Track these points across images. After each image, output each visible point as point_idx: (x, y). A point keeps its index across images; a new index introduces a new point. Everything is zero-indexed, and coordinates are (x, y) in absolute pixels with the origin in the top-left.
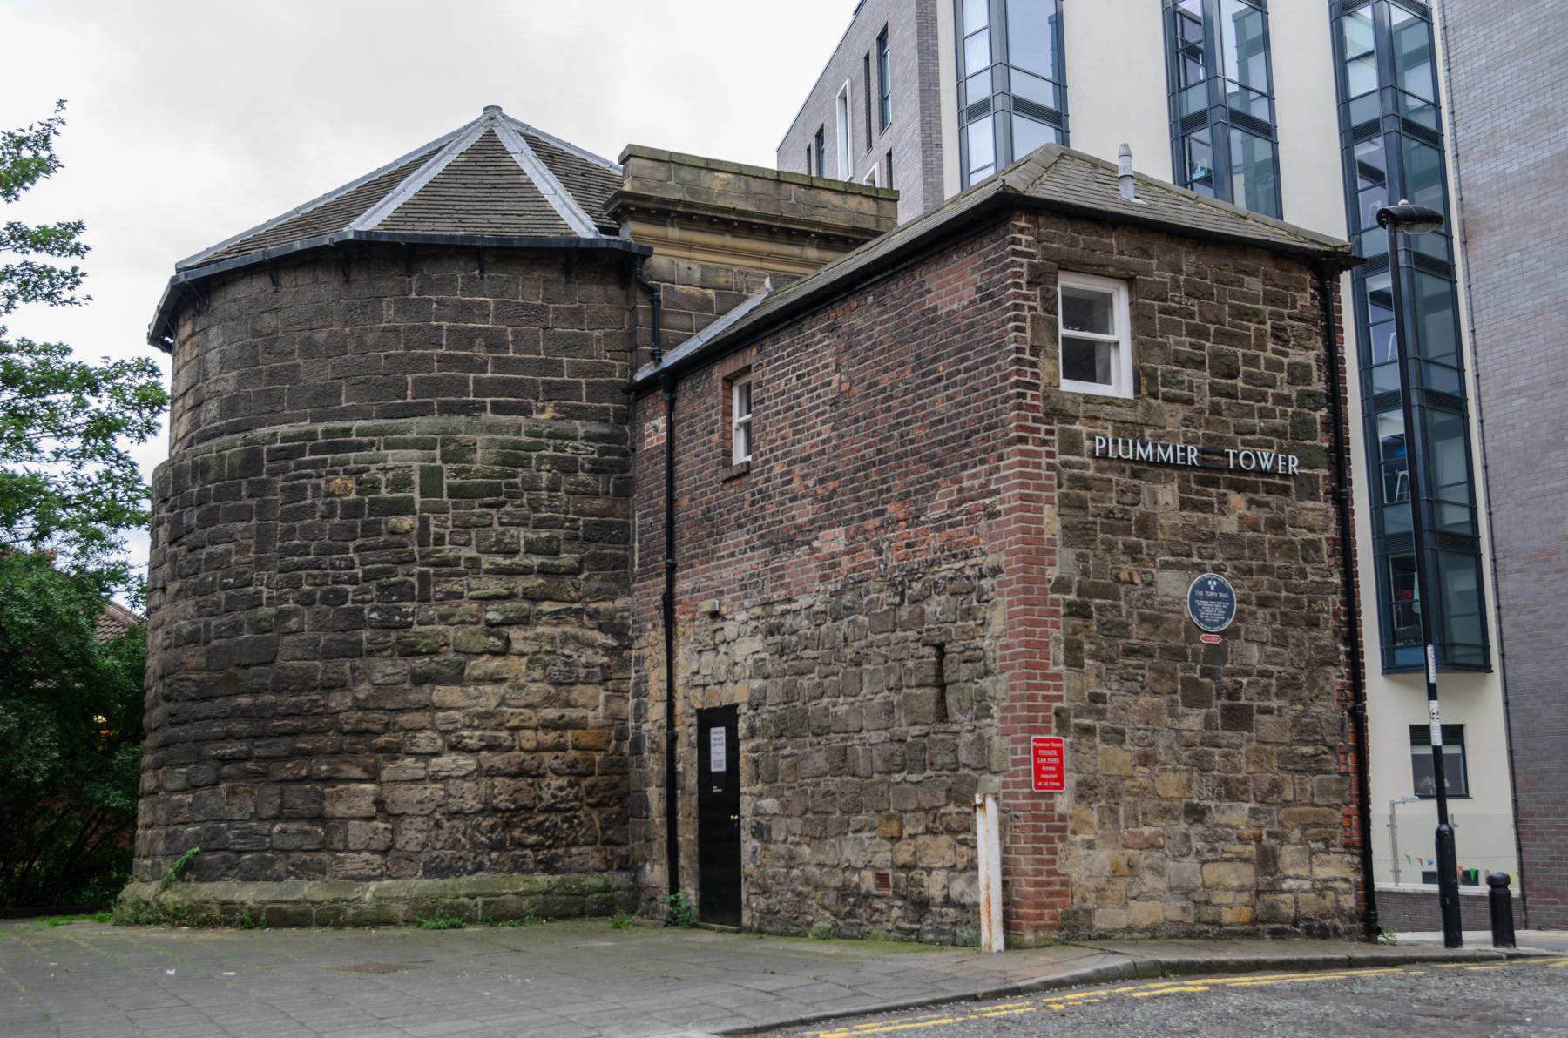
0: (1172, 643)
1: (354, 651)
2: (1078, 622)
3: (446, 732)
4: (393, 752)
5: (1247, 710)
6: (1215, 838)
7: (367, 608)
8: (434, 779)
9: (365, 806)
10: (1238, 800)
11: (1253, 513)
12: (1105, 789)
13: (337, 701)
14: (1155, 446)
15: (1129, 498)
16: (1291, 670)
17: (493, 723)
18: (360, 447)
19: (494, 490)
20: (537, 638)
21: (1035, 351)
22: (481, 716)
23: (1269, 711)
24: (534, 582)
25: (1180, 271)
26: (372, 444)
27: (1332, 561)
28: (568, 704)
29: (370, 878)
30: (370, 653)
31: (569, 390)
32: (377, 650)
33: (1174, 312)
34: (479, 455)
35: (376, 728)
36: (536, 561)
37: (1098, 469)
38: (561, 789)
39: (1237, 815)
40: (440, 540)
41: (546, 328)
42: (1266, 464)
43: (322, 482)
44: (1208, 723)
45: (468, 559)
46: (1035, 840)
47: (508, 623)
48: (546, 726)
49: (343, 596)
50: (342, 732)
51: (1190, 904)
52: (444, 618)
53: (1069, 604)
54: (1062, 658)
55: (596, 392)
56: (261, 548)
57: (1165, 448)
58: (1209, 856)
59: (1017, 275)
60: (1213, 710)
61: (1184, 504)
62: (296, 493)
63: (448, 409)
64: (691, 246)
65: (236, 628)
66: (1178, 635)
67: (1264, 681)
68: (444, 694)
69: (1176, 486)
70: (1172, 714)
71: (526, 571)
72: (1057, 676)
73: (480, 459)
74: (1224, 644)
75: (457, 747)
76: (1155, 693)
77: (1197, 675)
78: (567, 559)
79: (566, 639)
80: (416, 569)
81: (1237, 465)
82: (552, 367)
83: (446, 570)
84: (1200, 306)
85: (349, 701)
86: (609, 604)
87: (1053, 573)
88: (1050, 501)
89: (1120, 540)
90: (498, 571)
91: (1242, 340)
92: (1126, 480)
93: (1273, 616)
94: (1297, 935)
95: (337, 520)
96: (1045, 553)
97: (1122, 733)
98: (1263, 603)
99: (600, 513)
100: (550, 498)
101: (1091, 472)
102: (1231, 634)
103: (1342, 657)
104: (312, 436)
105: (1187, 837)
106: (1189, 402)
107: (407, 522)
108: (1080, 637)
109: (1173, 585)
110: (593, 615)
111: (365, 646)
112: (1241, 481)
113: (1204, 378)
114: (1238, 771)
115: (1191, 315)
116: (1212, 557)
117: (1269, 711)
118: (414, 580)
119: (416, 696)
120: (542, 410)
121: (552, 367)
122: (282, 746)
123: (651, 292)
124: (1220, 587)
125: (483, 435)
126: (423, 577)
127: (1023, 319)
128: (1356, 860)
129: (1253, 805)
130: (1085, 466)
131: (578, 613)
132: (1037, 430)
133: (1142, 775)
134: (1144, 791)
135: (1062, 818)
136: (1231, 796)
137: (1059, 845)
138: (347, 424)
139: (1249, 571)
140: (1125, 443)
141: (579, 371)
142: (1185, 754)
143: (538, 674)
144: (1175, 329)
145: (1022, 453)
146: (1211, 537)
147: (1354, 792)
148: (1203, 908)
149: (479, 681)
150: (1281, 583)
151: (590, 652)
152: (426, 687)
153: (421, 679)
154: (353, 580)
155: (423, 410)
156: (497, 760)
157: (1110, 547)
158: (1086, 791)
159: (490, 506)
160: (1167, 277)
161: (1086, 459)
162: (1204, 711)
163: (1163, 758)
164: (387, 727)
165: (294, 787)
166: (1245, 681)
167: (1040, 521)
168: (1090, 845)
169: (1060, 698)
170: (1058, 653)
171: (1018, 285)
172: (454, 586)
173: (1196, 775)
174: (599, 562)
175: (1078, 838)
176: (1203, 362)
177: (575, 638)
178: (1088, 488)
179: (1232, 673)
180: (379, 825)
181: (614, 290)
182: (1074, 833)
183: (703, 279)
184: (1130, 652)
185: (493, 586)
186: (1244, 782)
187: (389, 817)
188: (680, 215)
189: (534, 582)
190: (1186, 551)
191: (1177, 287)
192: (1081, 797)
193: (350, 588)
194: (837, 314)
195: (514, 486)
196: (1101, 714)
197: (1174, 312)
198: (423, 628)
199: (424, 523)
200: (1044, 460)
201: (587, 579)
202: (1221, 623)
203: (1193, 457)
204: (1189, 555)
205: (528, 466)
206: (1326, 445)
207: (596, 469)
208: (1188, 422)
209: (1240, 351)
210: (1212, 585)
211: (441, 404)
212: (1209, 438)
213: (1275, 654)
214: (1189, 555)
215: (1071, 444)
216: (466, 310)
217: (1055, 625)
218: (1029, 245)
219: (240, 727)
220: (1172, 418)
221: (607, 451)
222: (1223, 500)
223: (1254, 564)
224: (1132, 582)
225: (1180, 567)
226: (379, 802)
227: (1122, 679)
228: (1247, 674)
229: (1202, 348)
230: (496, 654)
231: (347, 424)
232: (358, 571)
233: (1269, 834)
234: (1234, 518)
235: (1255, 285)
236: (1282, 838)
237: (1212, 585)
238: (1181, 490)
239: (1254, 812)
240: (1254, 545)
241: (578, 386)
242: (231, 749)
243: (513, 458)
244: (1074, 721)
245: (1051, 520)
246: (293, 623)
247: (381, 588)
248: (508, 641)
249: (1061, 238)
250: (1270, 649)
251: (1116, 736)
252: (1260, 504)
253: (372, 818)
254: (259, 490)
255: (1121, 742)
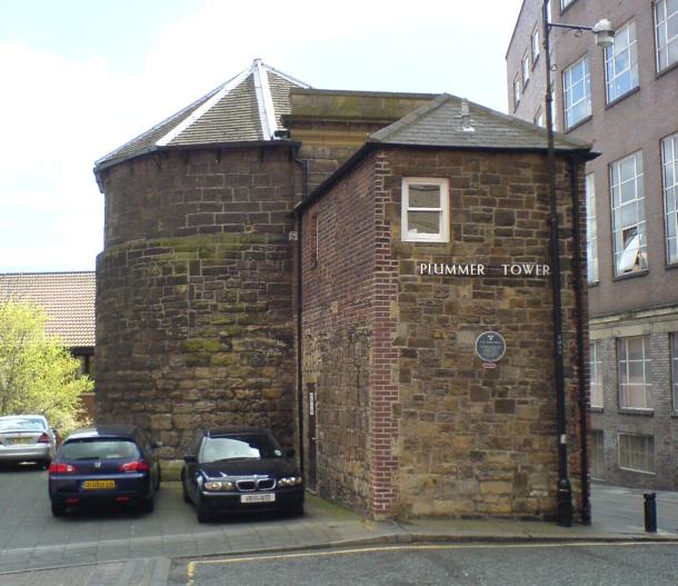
0: (466, 368)
1: (162, 350)
2: (408, 359)
3: (203, 390)
4: (179, 399)
5: (511, 403)
6: (487, 469)
7: (167, 330)
8: (196, 412)
9: (167, 425)
10: (502, 449)
11: (520, 298)
12: (422, 444)
13: (156, 375)
14: (457, 266)
15: (442, 294)
16: (541, 380)
17: (224, 385)
18: (164, 251)
19: (223, 271)
20: (245, 343)
21: (387, 223)
22: (218, 382)
23: (526, 403)
24: (243, 316)
25: (479, 171)
26: (169, 250)
27: (571, 321)
28: (261, 376)
29: (172, 459)
30: (169, 351)
31: (263, 217)
32: (172, 350)
33: (473, 193)
34: (217, 253)
35: (172, 387)
36: (245, 305)
37: (423, 281)
38: (257, 418)
39: (504, 458)
40: (199, 296)
41: (250, 187)
42: (528, 271)
43: (149, 269)
44: (486, 409)
45: (212, 306)
46: (378, 469)
47: (231, 336)
48: (250, 387)
49: (157, 325)
50: (157, 389)
51: (472, 503)
52: (201, 334)
53: (403, 351)
54: (397, 378)
55: (276, 217)
56: (126, 300)
57: (463, 267)
58: (483, 478)
59: (380, 183)
60: (489, 403)
61: (475, 296)
62: (139, 273)
63: (204, 231)
64: (324, 138)
65: (117, 338)
66: (469, 364)
67: (523, 387)
68: (202, 372)
69: (471, 286)
70: (464, 405)
71: (240, 310)
72: (395, 388)
73: (218, 256)
74: (498, 368)
75: (206, 397)
76: (453, 394)
77: (480, 385)
78: (260, 303)
79: (260, 344)
80: (189, 311)
81: (509, 272)
82: (254, 206)
83: (202, 311)
84: (491, 188)
85: (160, 375)
86: (282, 326)
87: (394, 336)
88: (393, 298)
89: (435, 317)
90: (226, 311)
91: (517, 204)
92: (440, 285)
93: (531, 352)
94: (538, 520)
95: (154, 288)
96: (391, 325)
97: (433, 416)
98: (524, 345)
99: (277, 280)
100: (252, 274)
101: (419, 282)
102: (504, 362)
103: (575, 373)
104: (144, 246)
105: (471, 468)
106: (481, 240)
107: (184, 288)
108: (409, 367)
109: (467, 338)
110: (275, 331)
111: (166, 348)
112: (512, 281)
113: (492, 227)
114: (504, 434)
115: (484, 194)
116: (493, 322)
117: (526, 403)
118: (188, 316)
119: (189, 372)
120: (249, 229)
121: (254, 206)
122: (134, 396)
123: (303, 167)
124: (496, 338)
125: (220, 245)
126: (192, 315)
127: (381, 206)
128: (579, 481)
129: (513, 452)
130: (415, 279)
131: (266, 331)
132: (388, 263)
133: (445, 436)
134: (445, 444)
135: (395, 458)
136: (498, 446)
137: (393, 472)
138: (158, 241)
139: (515, 329)
140: (439, 266)
141: (267, 207)
142: (471, 426)
143: (245, 362)
144: (475, 202)
145: (378, 275)
146: (493, 312)
147: (580, 445)
148: (480, 505)
149: (217, 365)
150: (537, 335)
151: (271, 350)
152: (193, 368)
153: (191, 365)
154: (161, 317)
155: (192, 232)
156: (226, 404)
157: (429, 320)
158: (410, 445)
159: (222, 278)
160: (470, 175)
161: (416, 276)
162: (484, 403)
163: (457, 428)
164: (176, 388)
165: (140, 414)
166: (510, 387)
167: (388, 309)
168: (410, 472)
169: (395, 399)
170: (395, 376)
171: (379, 189)
172: (206, 318)
173: (478, 437)
174: (276, 304)
175: (405, 468)
176: (491, 219)
177: (264, 343)
178: (417, 291)
179: (502, 384)
180: (173, 433)
181: (286, 165)
182: (402, 465)
183: (331, 155)
184: (440, 374)
185: (222, 319)
186: (508, 440)
187: (177, 430)
188: (316, 123)
189: (243, 316)
190: (473, 323)
191: (475, 179)
192: (407, 448)
193: (160, 320)
194: (332, 195)
195: (234, 268)
196: (421, 406)
197: (473, 193)
198: (192, 340)
199: (192, 288)
200: (391, 278)
201: (271, 313)
202: (496, 357)
203: (481, 270)
204: (478, 322)
205: (240, 258)
206: (571, 257)
207: (274, 258)
208: (480, 251)
209: (516, 210)
210: (491, 338)
211: (201, 229)
212: (493, 259)
213: (530, 373)
214: (478, 322)
215: (408, 268)
216: (216, 181)
217: (394, 362)
218: (385, 166)
219: (119, 385)
220: (471, 250)
221: (278, 249)
222: (501, 292)
223: (520, 325)
224: (442, 338)
225: (472, 329)
226: (173, 423)
227: (434, 388)
228: (511, 383)
229: (491, 210)
230: (225, 351)
231: (158, 241)
232: (163, 312)
233: (523, 467)
234: (507, 301)
235: (528, 173)
236: (531, 470)
237: (491, 338)
238: (474, 287)
239: (513, 456)
240: (520, 316)
241: (267, 215)
242: (116, 396)
243: (232, 255)
244: (403, 410)
245: (394, 309)
246: (138, 336)
247: (173, 321)
248: (231, 346)
249: (403, 162)
250: (527, 369)
251: (430, 417)
252: (524, 293)
253: (170, 430)
254: (125, 271)
255: (433, 420)
